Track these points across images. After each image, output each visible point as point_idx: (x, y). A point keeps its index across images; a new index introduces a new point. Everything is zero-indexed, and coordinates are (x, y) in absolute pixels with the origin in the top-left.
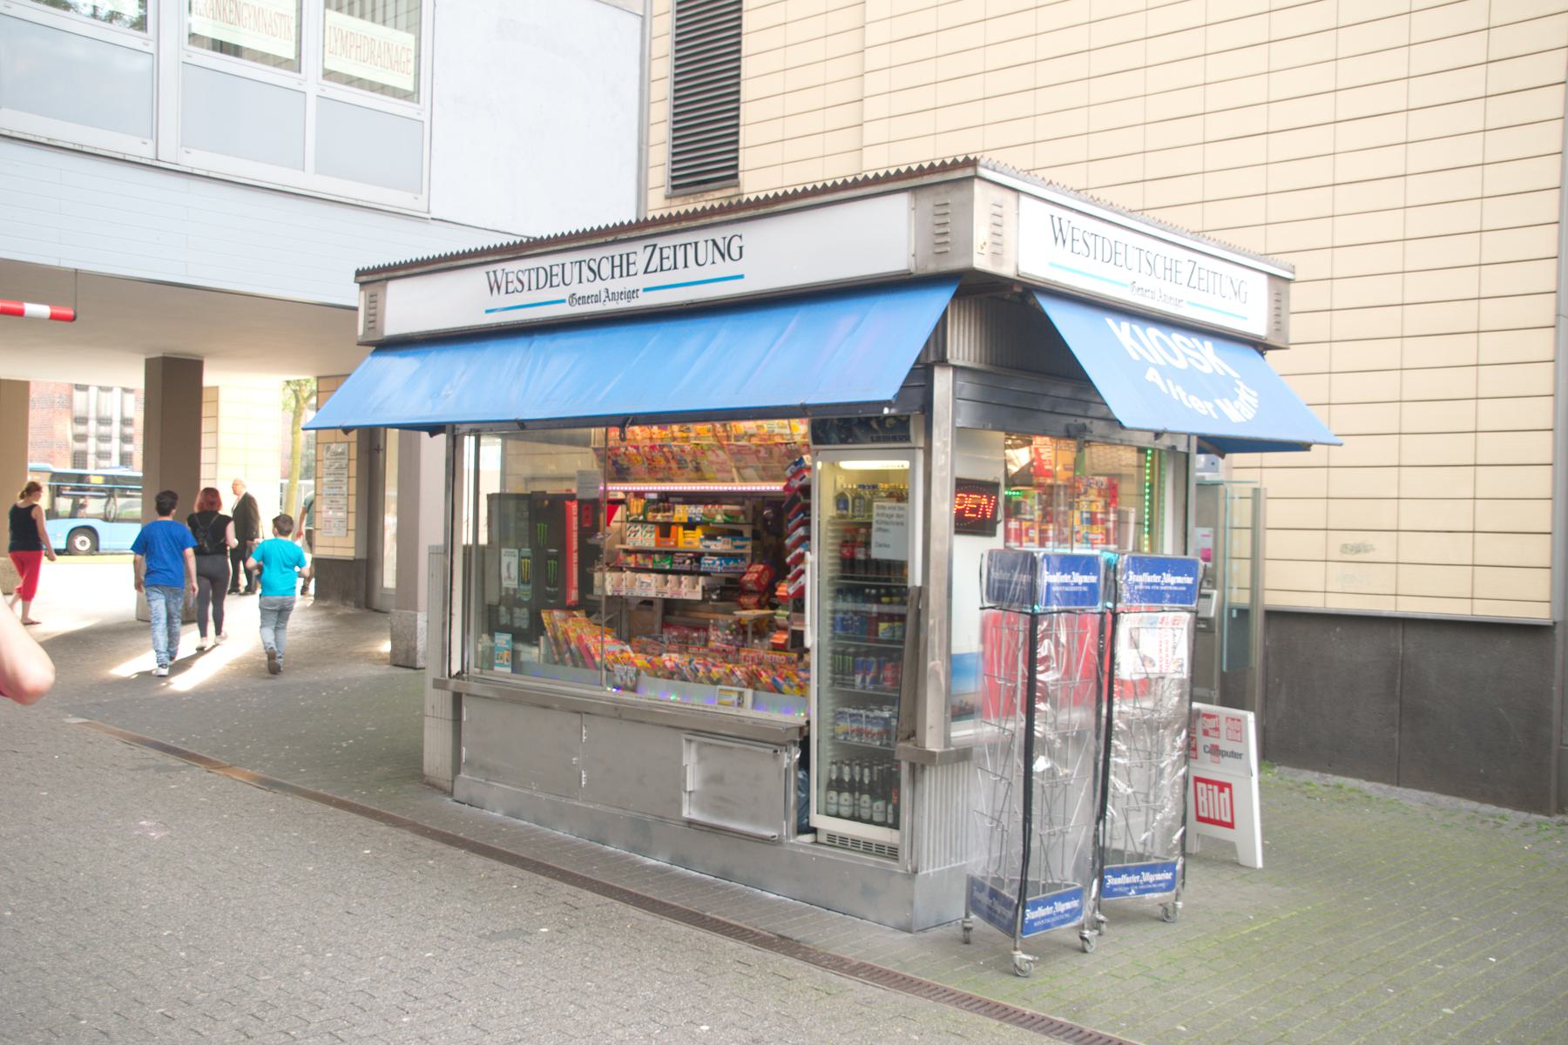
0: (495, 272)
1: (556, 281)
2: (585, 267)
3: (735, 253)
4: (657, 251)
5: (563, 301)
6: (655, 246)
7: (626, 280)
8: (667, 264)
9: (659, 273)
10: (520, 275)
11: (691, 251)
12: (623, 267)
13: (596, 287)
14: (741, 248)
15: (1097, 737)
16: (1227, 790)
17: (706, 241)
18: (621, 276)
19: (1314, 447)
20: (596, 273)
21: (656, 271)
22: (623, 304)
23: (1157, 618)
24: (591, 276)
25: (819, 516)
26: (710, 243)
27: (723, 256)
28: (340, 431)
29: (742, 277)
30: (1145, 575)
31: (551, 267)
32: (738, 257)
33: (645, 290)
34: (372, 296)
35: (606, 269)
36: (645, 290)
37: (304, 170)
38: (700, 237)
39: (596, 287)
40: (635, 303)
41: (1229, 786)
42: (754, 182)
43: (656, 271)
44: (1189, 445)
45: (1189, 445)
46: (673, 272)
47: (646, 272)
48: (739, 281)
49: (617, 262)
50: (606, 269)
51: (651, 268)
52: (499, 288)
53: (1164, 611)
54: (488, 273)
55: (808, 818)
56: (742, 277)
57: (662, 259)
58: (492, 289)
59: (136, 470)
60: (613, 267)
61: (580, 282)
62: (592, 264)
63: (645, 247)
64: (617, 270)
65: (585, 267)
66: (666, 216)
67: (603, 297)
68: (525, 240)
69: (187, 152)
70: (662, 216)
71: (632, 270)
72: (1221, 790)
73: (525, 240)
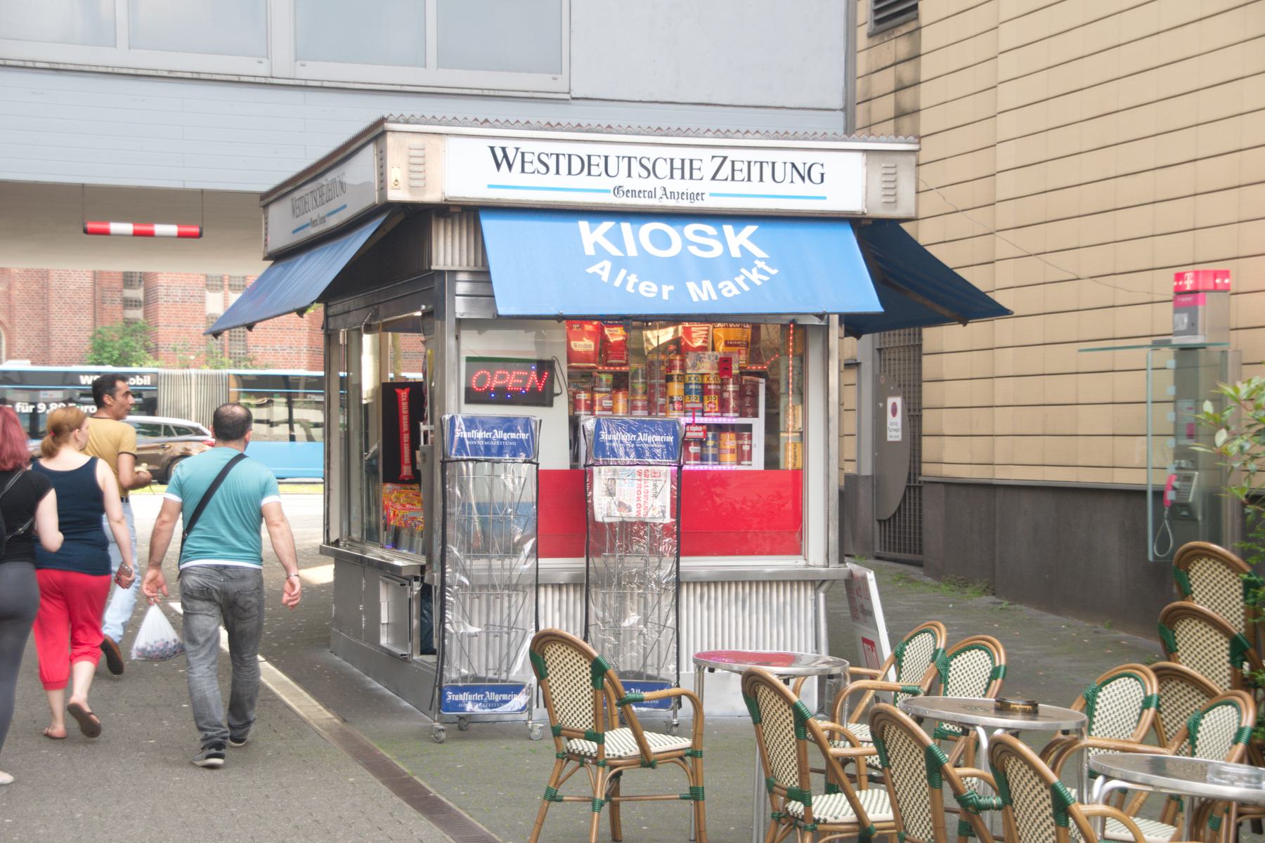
2: (635, 164)
3: (816, 176)
5: (608, 191)
6: (725, 158)
7: (687, 182)
8: (738, 175)
9: (729, 182)
13: (651, 184)
14: (822, 175)
15: (361, 437)
17: (618, 157)
20: (651, 171)
21: (726, 179)
23: (634, 470)
24: (645, 173)
25: (266, 235)
26: (789, 166)
27: (803, 178)
28: (295, 315)
29: (824, 198)
30: (929, 579)
31: (589, 157)
32: (819, 181)
36: (712, 195)
37: (425, 67)
39: (651, 184)
40: (698, 204)
43: (726, 179)
46: (746, 183)
47: (713, 178)
48: (824, 201)
50: (663, 169)
51: (720, 176)
52: (510, 166)
55: (115, 273)
56: (824, 198)
57: (733, 170)
58: (498, 166)
60: (672, 168)
62: (645, 162)
63: (713, 157)
67: (658, 194)
69: (302, 65)
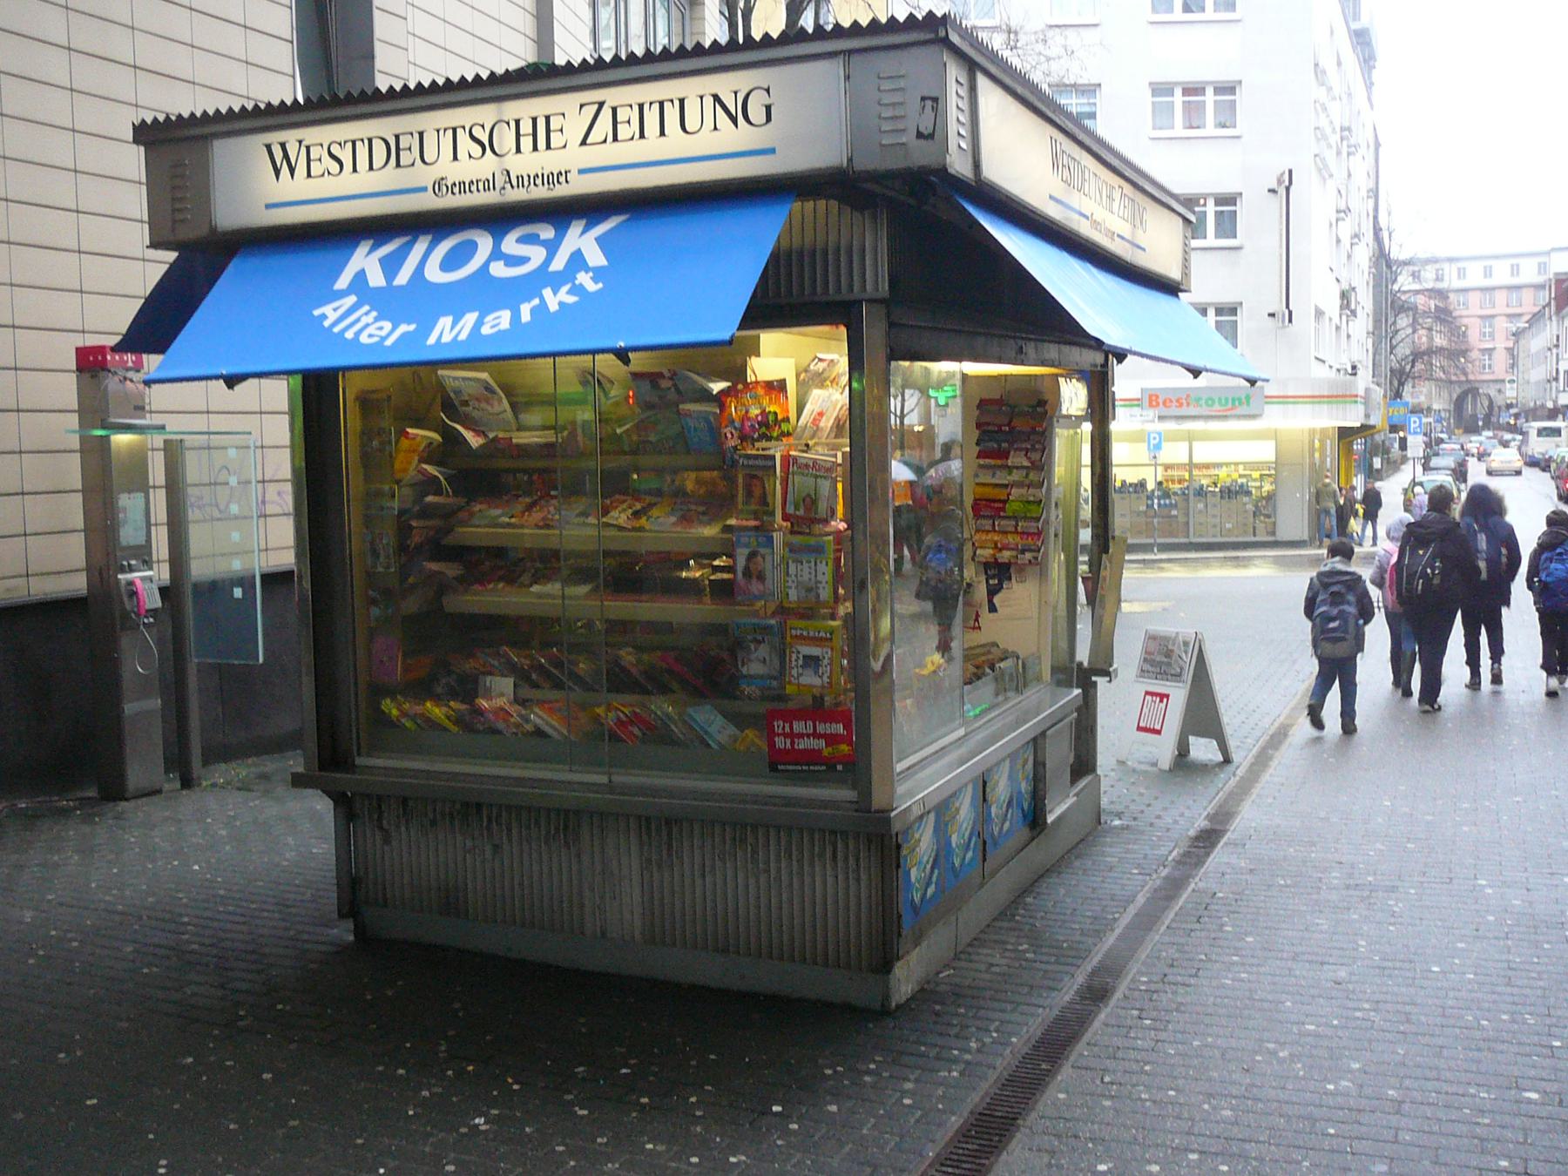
0: (283, 145)
1: (405, 158)
2: (463, 137)
4: (606, 114)
5: (425, 189)
6: (601, 104)
8: (623, 132)
10: (335, 150)
11: (672, 114)
12: (543, 134)
16: (1165, 700)
18: (535, 148)
19: (1130, 357)
22: (540, 193)
24: (477, 150)
26: (709, 101)
27: (734, 121)
31: (397, 137)
33: (581, 172)
34: (175, 166)
35: (505, 139)
38: (690, 88)
41: (1167, 696)
42: (391, 70)
44: (170, 433)
45: (170, 433)
47: (584, 143)
49: (526, 127)
50: (505, 139)
52: (292, 171)
53: (1188, 523)
54: (269, 147)
58: (277, 172)
59: (958, 393)
61: (455, 158)
62: (477, 132)
64: (526, 143)
65: (463, 137)
66: (149, 121)
68: (161, 118)
70: (243, 108)
71: (556, 139)
72: (1161, 701)
73: (161, 118)
